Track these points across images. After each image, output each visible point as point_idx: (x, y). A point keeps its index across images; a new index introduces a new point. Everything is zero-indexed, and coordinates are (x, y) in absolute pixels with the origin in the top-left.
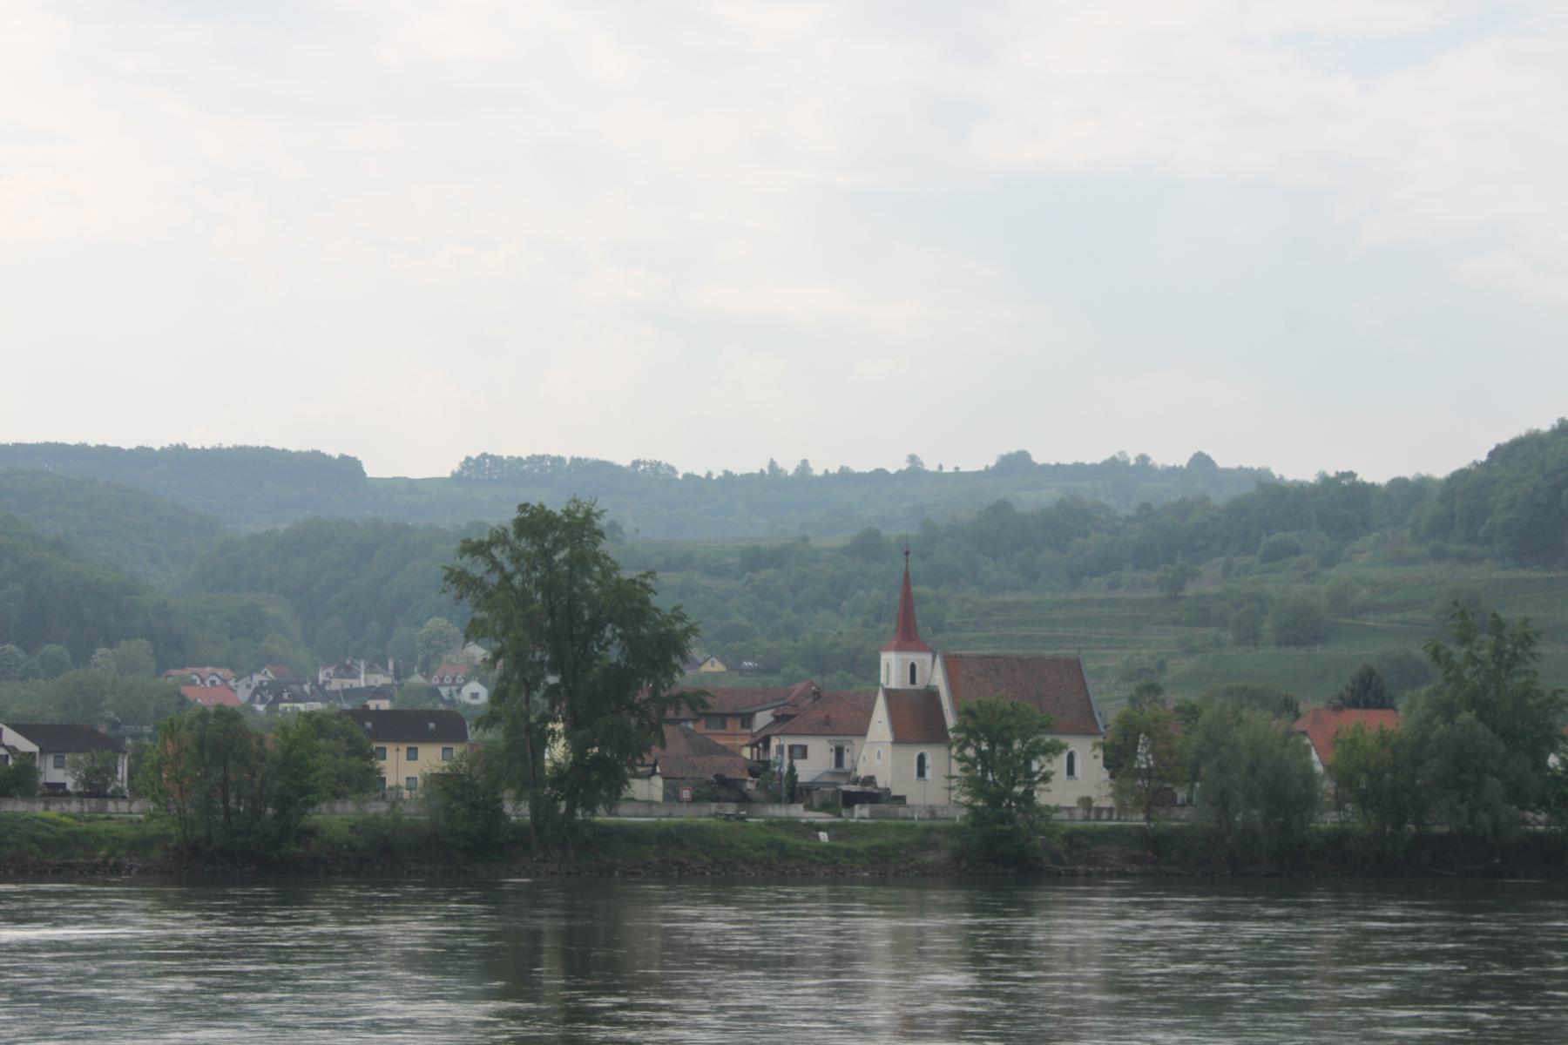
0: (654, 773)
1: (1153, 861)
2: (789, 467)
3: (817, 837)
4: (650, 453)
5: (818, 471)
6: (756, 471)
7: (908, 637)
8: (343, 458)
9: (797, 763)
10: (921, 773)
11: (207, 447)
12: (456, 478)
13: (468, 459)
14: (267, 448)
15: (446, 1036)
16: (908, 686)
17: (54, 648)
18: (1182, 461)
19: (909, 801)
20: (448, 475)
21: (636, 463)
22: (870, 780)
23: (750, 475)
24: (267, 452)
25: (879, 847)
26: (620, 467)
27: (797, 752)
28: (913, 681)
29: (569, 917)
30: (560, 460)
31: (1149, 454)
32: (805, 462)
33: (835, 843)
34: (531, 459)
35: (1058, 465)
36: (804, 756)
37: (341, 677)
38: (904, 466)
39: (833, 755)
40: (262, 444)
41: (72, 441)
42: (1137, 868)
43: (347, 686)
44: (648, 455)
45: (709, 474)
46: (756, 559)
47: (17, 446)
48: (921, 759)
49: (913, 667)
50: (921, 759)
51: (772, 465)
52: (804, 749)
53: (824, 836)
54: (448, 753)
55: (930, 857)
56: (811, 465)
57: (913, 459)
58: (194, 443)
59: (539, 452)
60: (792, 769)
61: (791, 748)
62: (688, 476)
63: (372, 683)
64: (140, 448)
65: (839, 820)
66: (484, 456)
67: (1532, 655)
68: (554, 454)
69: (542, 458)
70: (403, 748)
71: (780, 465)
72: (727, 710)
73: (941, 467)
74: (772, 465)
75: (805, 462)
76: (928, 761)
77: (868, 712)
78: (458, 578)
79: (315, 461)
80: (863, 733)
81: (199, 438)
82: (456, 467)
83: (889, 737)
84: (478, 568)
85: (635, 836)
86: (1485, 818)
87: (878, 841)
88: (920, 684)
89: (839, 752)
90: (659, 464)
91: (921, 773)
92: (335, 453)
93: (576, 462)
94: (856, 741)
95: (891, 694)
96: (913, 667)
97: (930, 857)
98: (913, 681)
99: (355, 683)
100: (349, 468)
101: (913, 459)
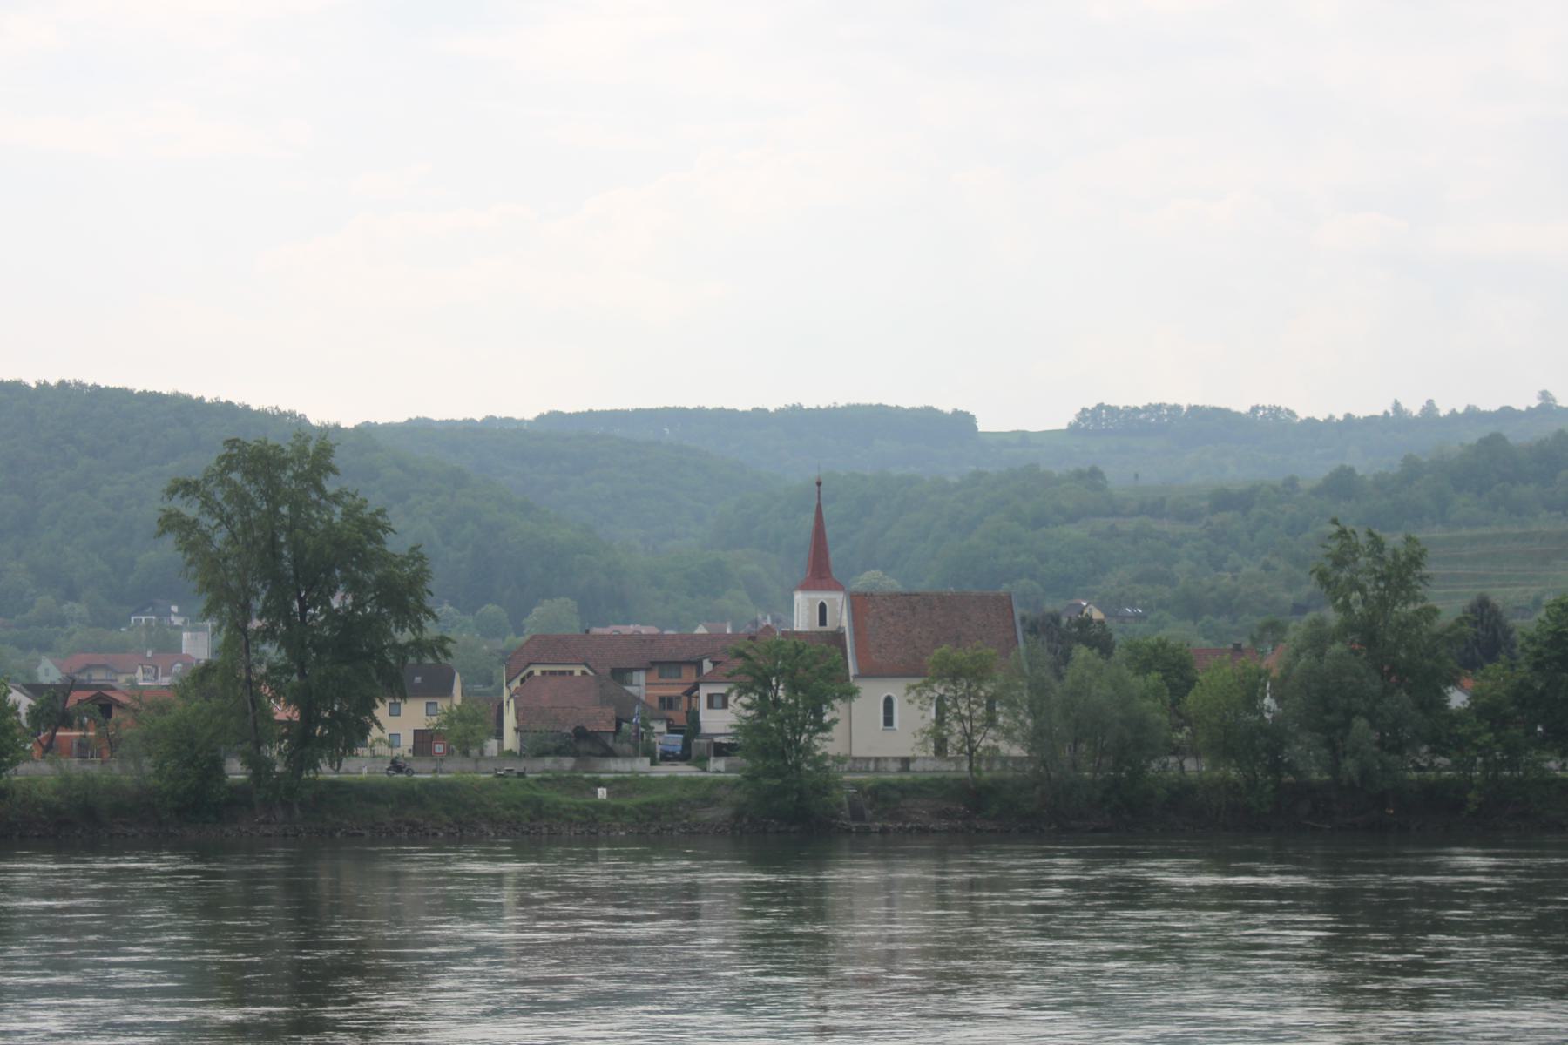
1: (963, 816)
2: (1414, 408)
3: (595, 793)
4: (1268, 397)
5: (1443, 411)
6: (1380, 413)
7: (819, 573)
8: (956, 412)
10: (888, 721)
11: (822, 407)
12: (1073, 429)
13: (1084, 410)
14: (880, 406)
15: (157, 1013)
16: (817, 627)
17: (491, 608)
20: (1064, 427)
21: (1255, 409)
23: (1374, 418)
24: (881, 409)
25: (653, 804)
26: (1238, 414)
28: (823, 621)
29: (820, 887)
30: (1177, 408)
32: (1430, 402)
33: (614, 802)
34: (1147, 409)
35: (63, 384)
38: (1535, 403)
40: (875, 403)
41: (691, 405)
42: (944, 824)
44: (1267, 401)
46: (1224, 500)
47: (638, 412)
48: (888, 703)
49: (822, 607)
51: (1397, 406)
53: (602, 793)
54: (432, 709)
55: (708, 815)
56: (1438, 405)
57: (1544, 395)
58: (809, 403)
59: (1156, 401)
64: (756, 410)
65: (702, 774)
66: (1101, 406)
67: (1421, 578)
68: (1171, 402)
69: (1159, 407)
71: (1405, 405)
72: (681, 658)
74: (1397, 406)
75: (1430, 402)
78: (171, 523)
79: (928, 416)
81: (816, 397)
82: (1072, 418)
84: (191, 509)
85: (366, 794)
86: (1350, 765)
87: (656, 797)
88: (830, 626)
90: (1279, 409)
91: (888, 721)
92: (947, 408)
93: (1194, 409)
96: (822, 607)
97: (708, 815)
98: (823, 621)
100: (962, 422)
101: (1544, 395)
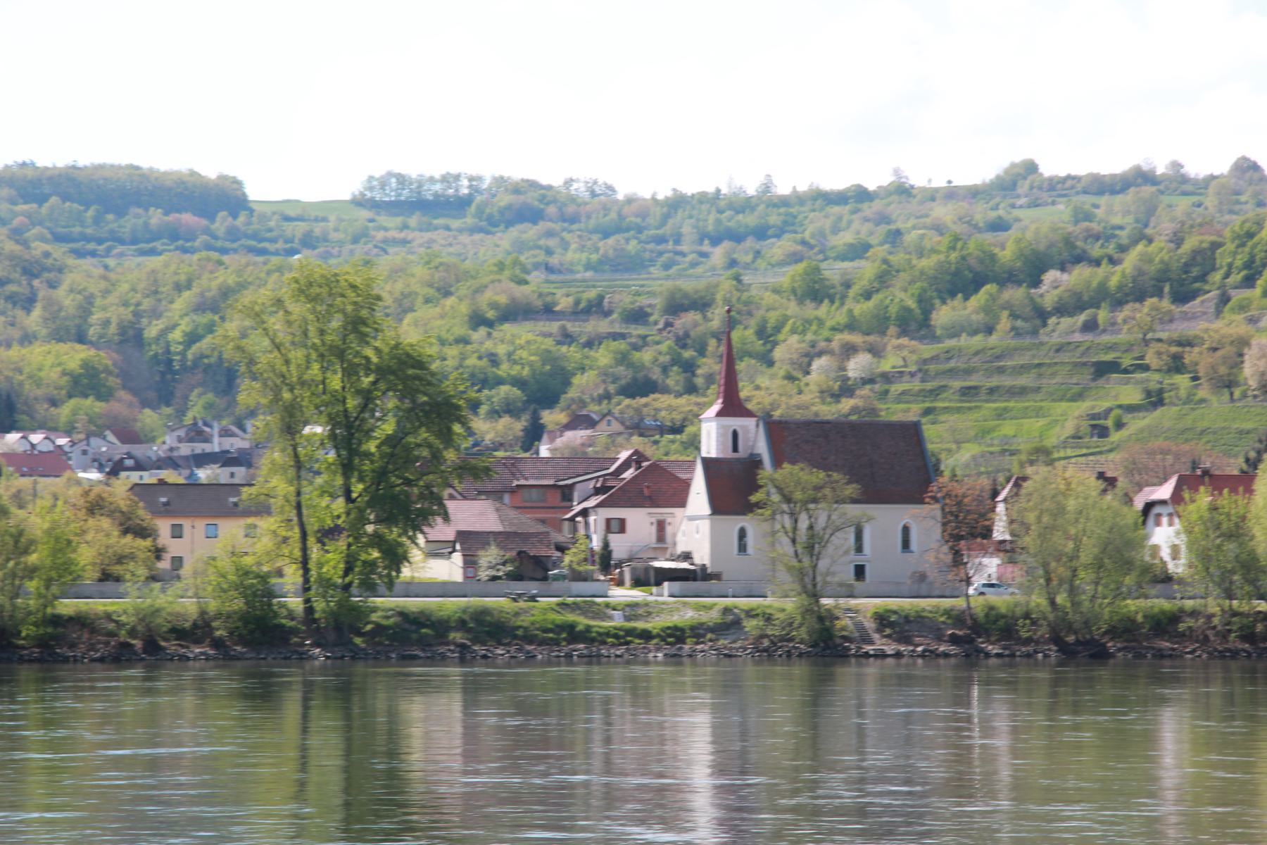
0: (454, 551)
9: (612, 537)
16: (729, 454)
18: (1221, 166)
19: (724, 577)
22: (687, 556)
27: (615, 525)
28: (735, 449)
31: (1181, 160)
36: (622, 529)
37: (191, 440)
39: (654, 529)
43: (198, 451)
45: (718, 191)
48: (742, 534)
49: (735, 434)
50: (742, 534)
52: (622, 522)
57: (896, 172)
60: (606, 545)
61: (608, 521)
62: (630, 200)
63: (227, 447)
70: (201, 524)
73: (930, 181)
76: (750, 540)
77: (686, 485)
80: (682, 503)
83: (706, 510)
89: (661, 526)
91: (742, 548)
94: (677, 511)
95: (707, 463)
96: (735, 434)
98: (735, 449)
99: (207, 447)
101: (674, 190)
